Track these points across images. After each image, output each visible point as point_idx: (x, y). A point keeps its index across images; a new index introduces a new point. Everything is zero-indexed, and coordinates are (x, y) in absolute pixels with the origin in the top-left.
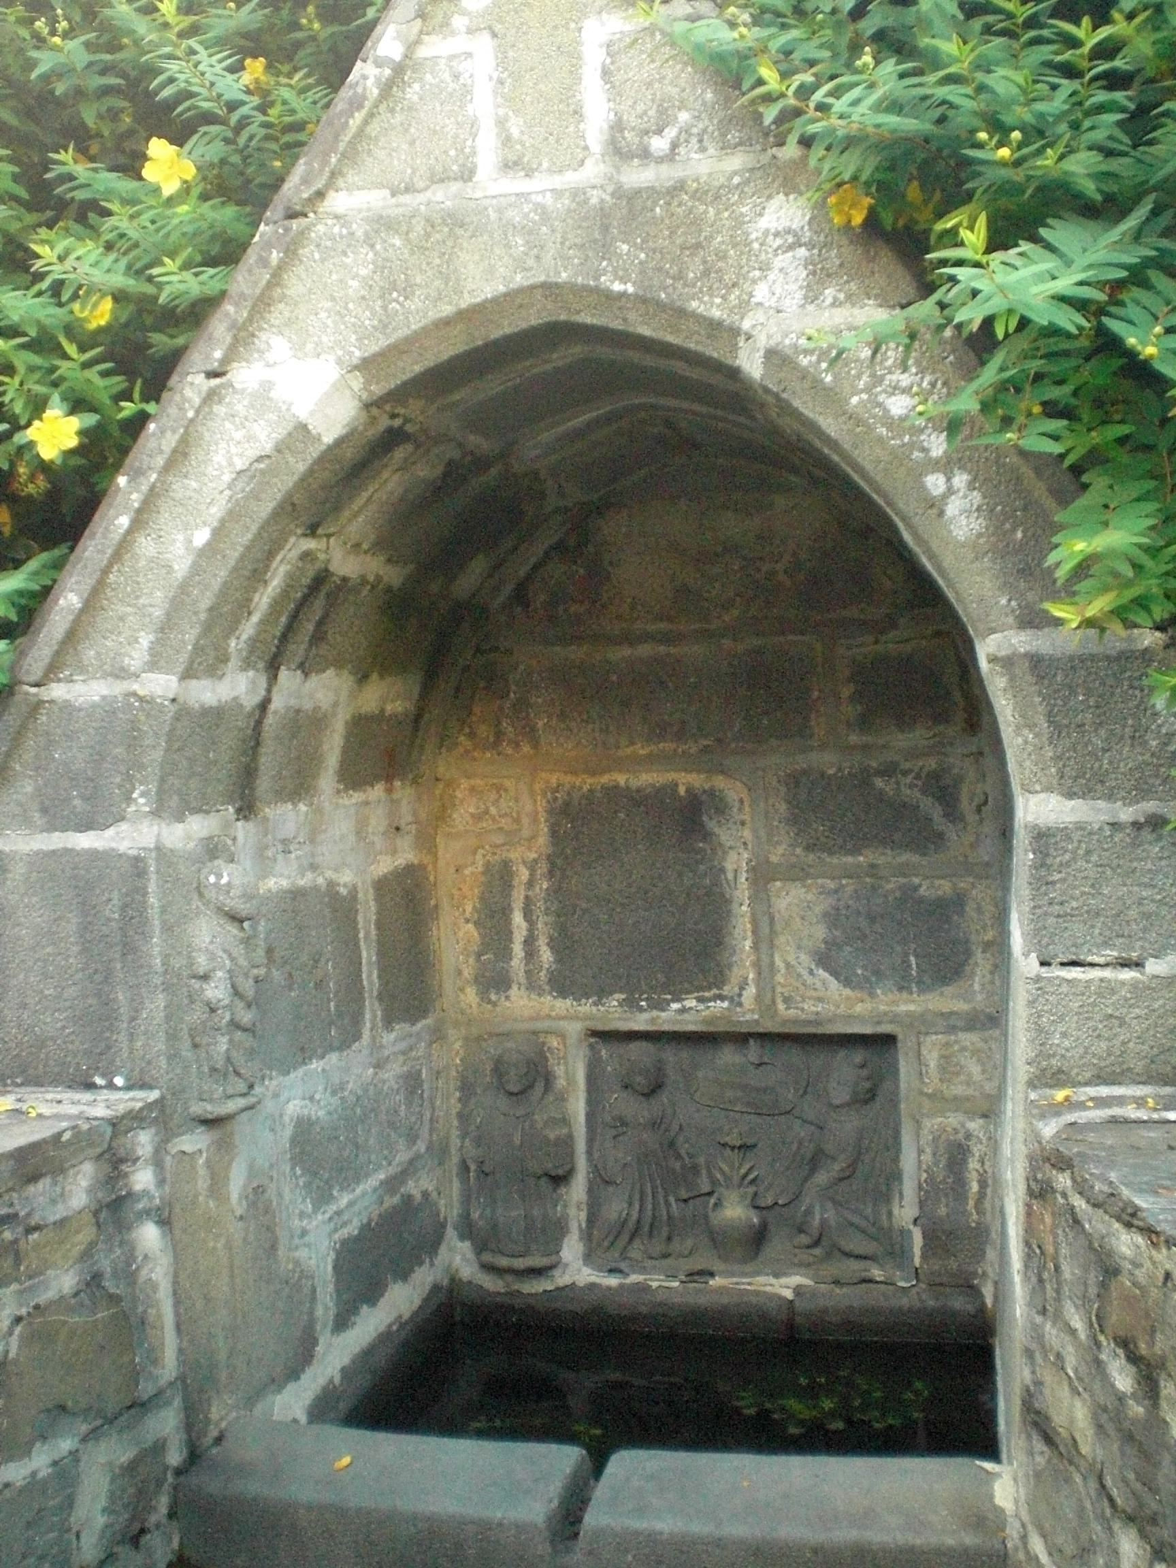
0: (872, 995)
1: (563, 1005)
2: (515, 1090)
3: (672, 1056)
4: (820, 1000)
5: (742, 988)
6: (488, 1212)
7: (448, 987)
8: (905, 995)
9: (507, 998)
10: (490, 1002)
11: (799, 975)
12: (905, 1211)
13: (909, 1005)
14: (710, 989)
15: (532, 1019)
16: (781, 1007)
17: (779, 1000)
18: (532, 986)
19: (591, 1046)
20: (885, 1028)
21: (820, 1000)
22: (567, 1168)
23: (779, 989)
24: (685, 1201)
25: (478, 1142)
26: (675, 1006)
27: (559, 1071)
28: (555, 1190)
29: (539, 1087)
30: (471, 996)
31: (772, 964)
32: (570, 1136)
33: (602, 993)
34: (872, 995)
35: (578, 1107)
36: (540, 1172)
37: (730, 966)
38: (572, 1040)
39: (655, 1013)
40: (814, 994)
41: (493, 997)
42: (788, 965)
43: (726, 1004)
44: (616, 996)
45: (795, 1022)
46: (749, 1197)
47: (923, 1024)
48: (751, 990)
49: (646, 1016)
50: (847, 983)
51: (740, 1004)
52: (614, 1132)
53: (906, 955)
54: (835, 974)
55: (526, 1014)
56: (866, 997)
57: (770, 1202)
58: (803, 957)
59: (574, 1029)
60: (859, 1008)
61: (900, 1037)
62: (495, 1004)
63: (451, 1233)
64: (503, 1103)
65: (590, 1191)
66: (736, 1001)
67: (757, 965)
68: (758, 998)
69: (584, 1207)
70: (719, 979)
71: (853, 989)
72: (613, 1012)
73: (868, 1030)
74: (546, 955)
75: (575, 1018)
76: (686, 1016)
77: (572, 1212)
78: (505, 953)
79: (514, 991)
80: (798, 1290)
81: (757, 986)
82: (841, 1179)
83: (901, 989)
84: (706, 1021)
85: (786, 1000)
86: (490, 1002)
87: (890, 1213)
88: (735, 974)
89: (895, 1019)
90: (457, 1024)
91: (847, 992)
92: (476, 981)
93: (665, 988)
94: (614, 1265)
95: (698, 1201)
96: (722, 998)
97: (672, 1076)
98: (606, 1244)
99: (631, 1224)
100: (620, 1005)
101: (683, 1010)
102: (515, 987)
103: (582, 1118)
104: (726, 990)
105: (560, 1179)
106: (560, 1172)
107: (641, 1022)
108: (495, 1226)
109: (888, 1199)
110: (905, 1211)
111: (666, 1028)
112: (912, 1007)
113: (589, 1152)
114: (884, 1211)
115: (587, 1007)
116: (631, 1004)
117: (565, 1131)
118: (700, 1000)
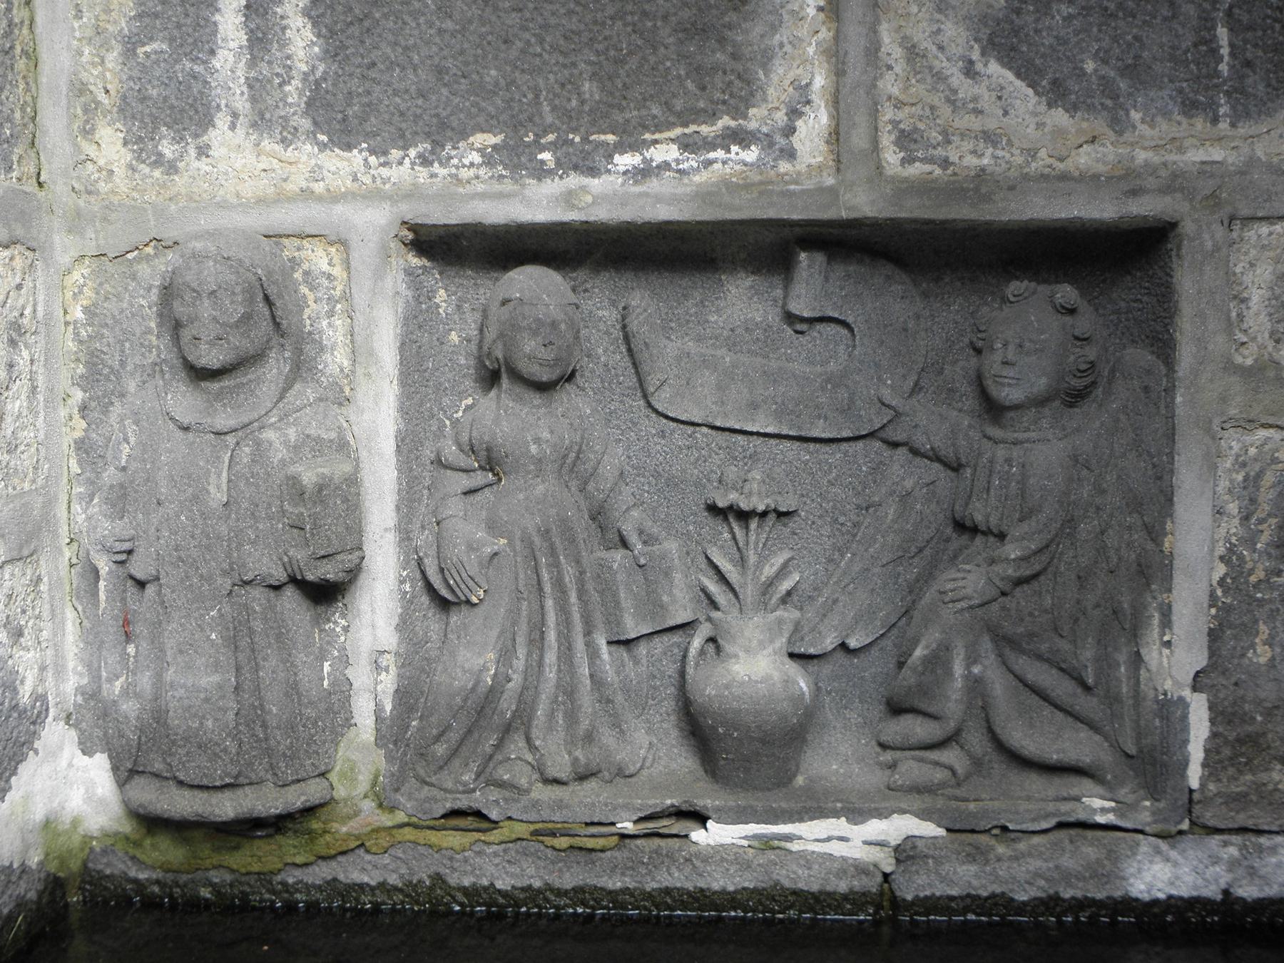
0: (1118, 124)
1: (344, 166)
2: (210, 357)
3: (596, 308)
4: (990, 138)
5: (794, 113)
6: (145, 681)
7: (55, 123)
8: (1199, 124)
9: (203, 151)
10: (159, 161)
11: (939, 77)
12: (1174, 659)
13: (1206, 147)
14: (713, 117)
15: (261, 201)
16: (891, 157)
17: (887, 139)
18: (263, 119)
19: (409, 272)
20: (1146, 207)
21: (990, 138)
22: (349, 560)
23: (888, 114)
24: (627, 643)
25: (120, 501)
26: (626, 161)
27: (334, 332)
28: (317, 621)
29: (274, 369)
30: (110, 146)
31: (873, 51)
32: (353, 481)
33: (441, 134)
34: (1118, 124)
35: (377, 418)
36: (280, 575)
37: (766, 59)
38: (364, 254)
39: (574, 180)
40: (975, 123)
41: (168, 149)
42: (913, 52)
43: (751, 155)
44: (480, 139)
45: (923, 187)
46: (788, 629)
47: (1235, 203)
48: (812, 131)
49: (552, 187)
50: (1057, 94)
51: (790, 154)
52: (466, 482)
53: (1207, 23)
54: (1028, 73)
55: (249, 190)
56: (1099, 124)
57: (829, 642)
58: (954, 32)
59: (373, 223)
60: (1085, 159)
61: (1188, 227)
62: (172, 168)
63: (57, 736)
64: (183, 401)
65: (404, 625)
66: (780, 144)
67: (836, 56)
68: (836, 136)
69: (387, 660)
70: (742, 94)
71: (1072, 109)
72: (476, 185)
73: (1102, 209)
74: (301, 41)
75: (373, 196)
76: (653, 185)
77: (360, 675)
78: (198, 39)
79: (220, 135)
80: (906, 852)
81: (835, 101)
82: (1019, 582)
83: (1190, 107)
84: (705, 195)
85: (906, 139)
86: (159, 161)
87: (1137, 660)
88: (777, 84)
89: (1175, 182)
90: (76, 222)
91: (1059, 117)
92: (125, 109)
93: (600, 117)
94: (463, 803)
95: (659, 644)
96: (740, 137)
97: (603, 352)
98: (440, 750)
99: (507, 705)
100: (488, 162)
101: (644, 172)
102: (222, 121)
103: (388, 446)
104: (756, 119)
105: (325, 594)
106: (329, 572)
107: (540, 201)
108: (160, 716)
109: (1135, 633)
110: (1174, 659)
111: (601, 214)
112: (1217, 154)
113: (404, 536)
114: (1122, 657)
115: (403, 170)
116: (515, 159)
117: (347, 468)
118: (687, 145)
